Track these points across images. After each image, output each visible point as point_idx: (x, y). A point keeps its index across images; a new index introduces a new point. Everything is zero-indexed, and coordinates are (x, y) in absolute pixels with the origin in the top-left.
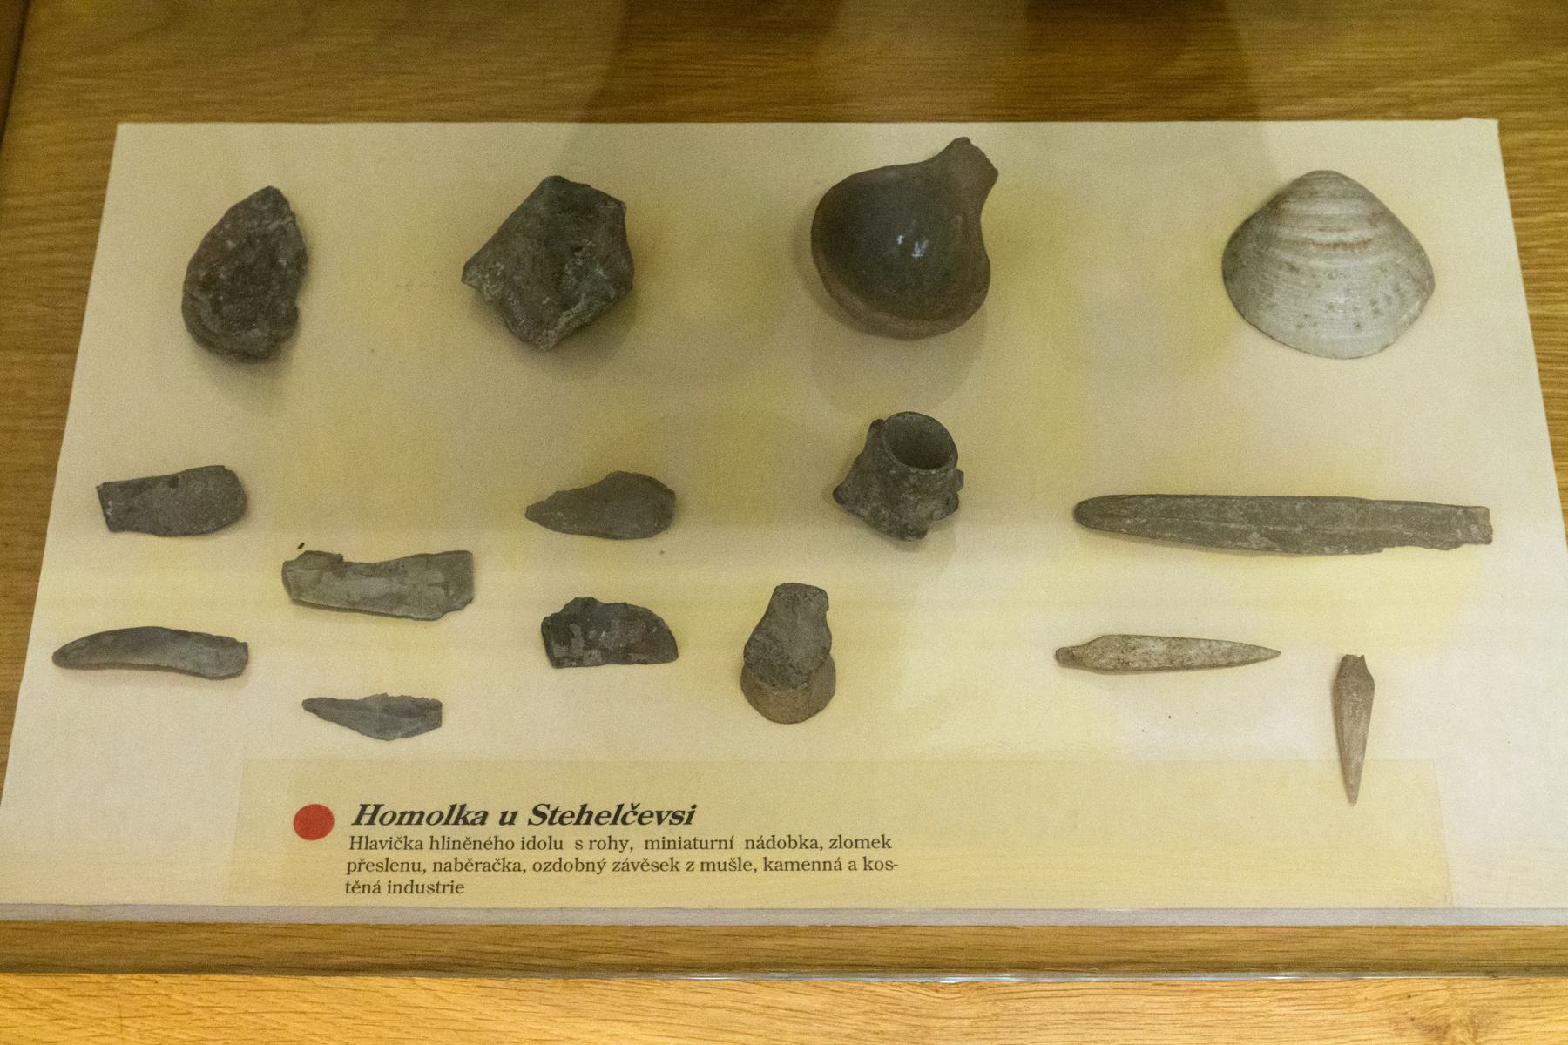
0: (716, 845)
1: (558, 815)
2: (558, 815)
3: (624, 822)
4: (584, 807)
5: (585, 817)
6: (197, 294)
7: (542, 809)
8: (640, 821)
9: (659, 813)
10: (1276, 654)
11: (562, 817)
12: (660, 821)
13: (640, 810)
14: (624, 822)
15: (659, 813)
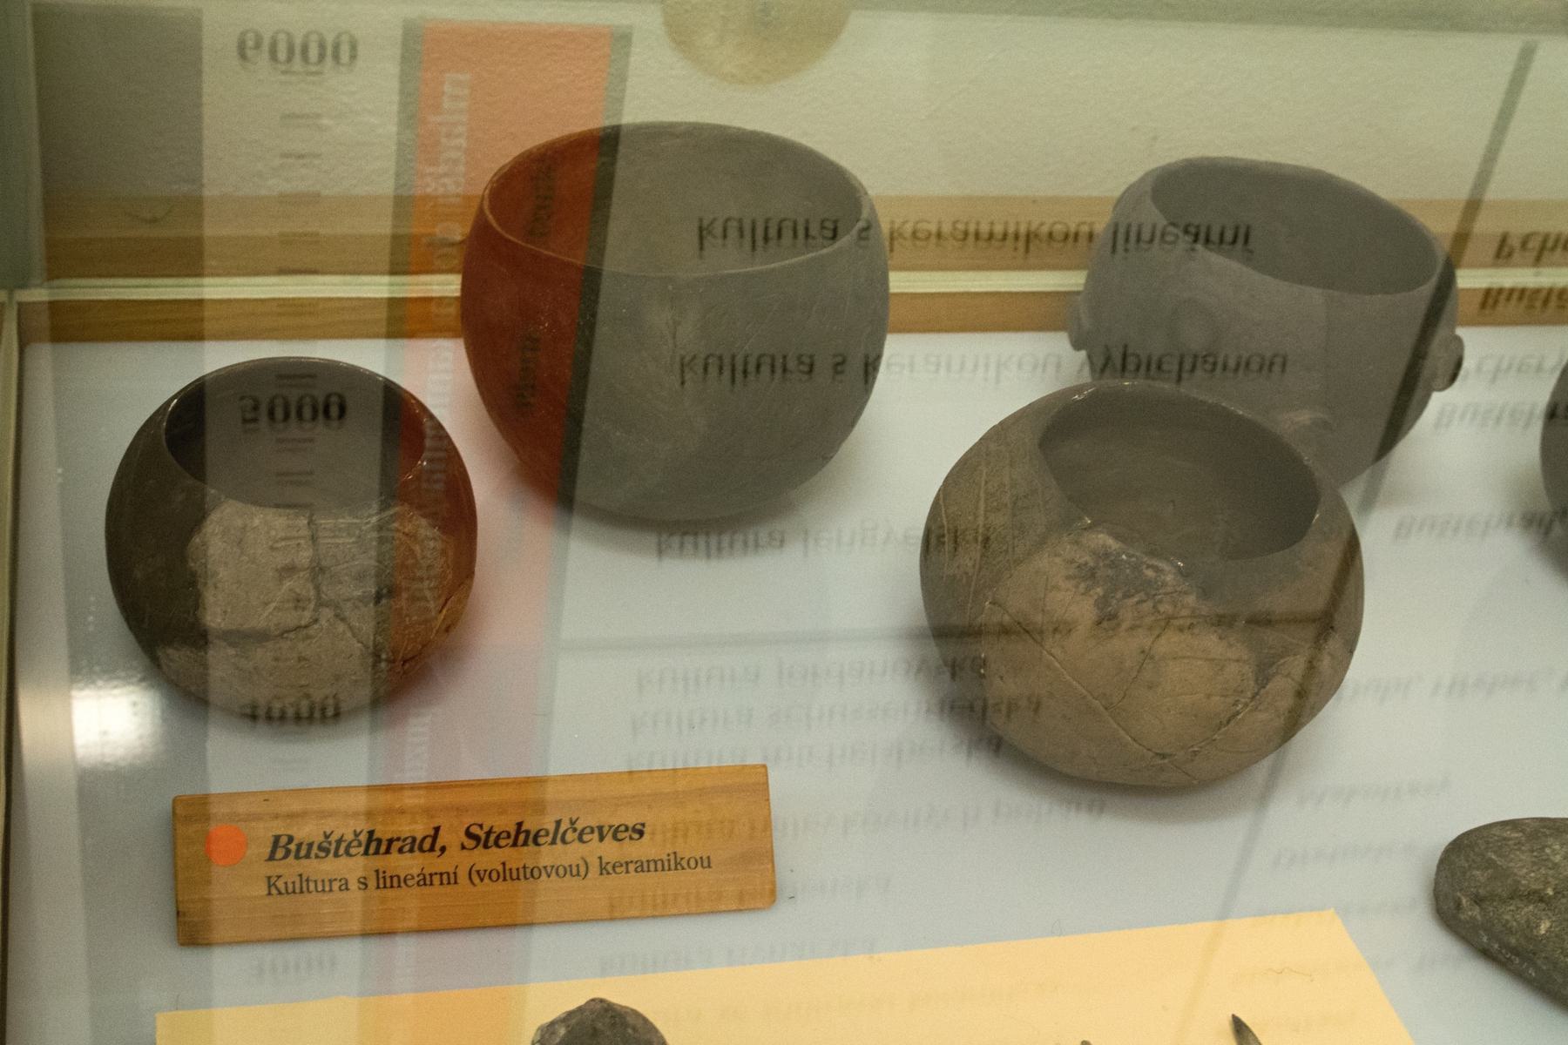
0: (436, 879)
1: (343, 845)
2: (343, 845)
3: (564, 841)
4: (520, 825)
5: (522, 837)
6: (1125, 626)
7: (475, 830)
8: (580, 839)
9: (600, 828)
10: (701, 257)
11: (498, 838)
12: (602, 839)
13: (579, 826)
14: (564, 841)
15: (600, 828)
